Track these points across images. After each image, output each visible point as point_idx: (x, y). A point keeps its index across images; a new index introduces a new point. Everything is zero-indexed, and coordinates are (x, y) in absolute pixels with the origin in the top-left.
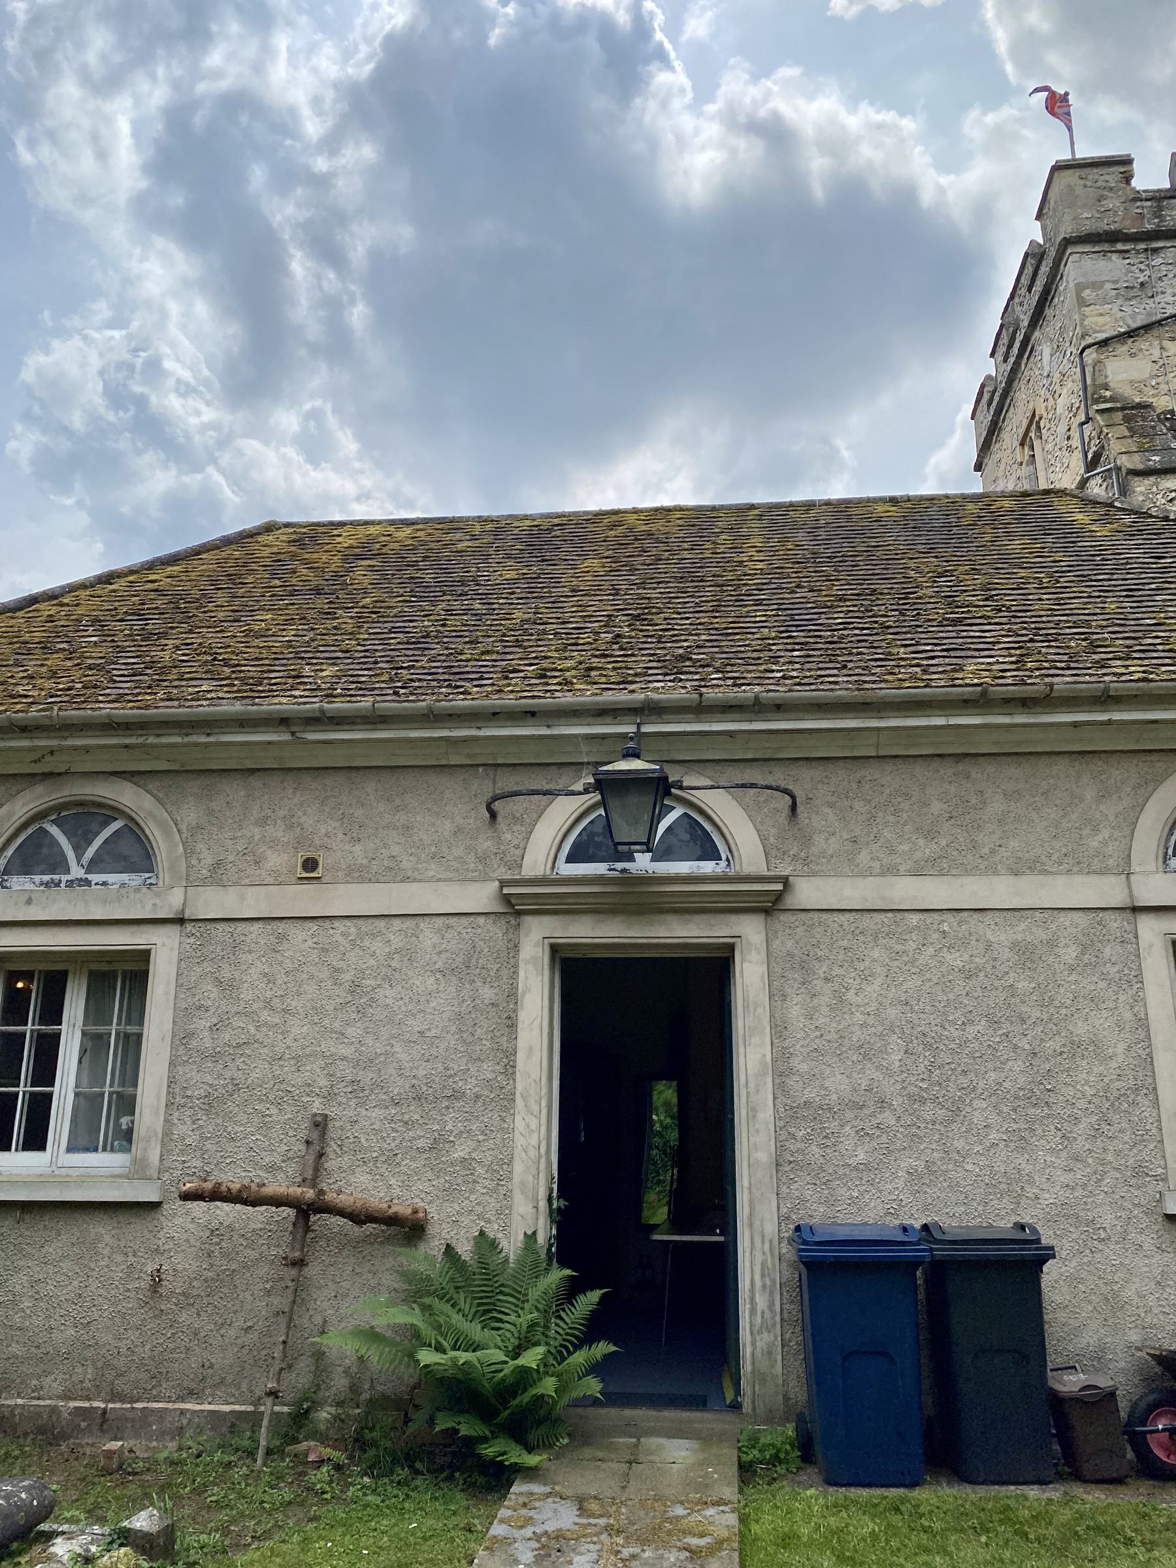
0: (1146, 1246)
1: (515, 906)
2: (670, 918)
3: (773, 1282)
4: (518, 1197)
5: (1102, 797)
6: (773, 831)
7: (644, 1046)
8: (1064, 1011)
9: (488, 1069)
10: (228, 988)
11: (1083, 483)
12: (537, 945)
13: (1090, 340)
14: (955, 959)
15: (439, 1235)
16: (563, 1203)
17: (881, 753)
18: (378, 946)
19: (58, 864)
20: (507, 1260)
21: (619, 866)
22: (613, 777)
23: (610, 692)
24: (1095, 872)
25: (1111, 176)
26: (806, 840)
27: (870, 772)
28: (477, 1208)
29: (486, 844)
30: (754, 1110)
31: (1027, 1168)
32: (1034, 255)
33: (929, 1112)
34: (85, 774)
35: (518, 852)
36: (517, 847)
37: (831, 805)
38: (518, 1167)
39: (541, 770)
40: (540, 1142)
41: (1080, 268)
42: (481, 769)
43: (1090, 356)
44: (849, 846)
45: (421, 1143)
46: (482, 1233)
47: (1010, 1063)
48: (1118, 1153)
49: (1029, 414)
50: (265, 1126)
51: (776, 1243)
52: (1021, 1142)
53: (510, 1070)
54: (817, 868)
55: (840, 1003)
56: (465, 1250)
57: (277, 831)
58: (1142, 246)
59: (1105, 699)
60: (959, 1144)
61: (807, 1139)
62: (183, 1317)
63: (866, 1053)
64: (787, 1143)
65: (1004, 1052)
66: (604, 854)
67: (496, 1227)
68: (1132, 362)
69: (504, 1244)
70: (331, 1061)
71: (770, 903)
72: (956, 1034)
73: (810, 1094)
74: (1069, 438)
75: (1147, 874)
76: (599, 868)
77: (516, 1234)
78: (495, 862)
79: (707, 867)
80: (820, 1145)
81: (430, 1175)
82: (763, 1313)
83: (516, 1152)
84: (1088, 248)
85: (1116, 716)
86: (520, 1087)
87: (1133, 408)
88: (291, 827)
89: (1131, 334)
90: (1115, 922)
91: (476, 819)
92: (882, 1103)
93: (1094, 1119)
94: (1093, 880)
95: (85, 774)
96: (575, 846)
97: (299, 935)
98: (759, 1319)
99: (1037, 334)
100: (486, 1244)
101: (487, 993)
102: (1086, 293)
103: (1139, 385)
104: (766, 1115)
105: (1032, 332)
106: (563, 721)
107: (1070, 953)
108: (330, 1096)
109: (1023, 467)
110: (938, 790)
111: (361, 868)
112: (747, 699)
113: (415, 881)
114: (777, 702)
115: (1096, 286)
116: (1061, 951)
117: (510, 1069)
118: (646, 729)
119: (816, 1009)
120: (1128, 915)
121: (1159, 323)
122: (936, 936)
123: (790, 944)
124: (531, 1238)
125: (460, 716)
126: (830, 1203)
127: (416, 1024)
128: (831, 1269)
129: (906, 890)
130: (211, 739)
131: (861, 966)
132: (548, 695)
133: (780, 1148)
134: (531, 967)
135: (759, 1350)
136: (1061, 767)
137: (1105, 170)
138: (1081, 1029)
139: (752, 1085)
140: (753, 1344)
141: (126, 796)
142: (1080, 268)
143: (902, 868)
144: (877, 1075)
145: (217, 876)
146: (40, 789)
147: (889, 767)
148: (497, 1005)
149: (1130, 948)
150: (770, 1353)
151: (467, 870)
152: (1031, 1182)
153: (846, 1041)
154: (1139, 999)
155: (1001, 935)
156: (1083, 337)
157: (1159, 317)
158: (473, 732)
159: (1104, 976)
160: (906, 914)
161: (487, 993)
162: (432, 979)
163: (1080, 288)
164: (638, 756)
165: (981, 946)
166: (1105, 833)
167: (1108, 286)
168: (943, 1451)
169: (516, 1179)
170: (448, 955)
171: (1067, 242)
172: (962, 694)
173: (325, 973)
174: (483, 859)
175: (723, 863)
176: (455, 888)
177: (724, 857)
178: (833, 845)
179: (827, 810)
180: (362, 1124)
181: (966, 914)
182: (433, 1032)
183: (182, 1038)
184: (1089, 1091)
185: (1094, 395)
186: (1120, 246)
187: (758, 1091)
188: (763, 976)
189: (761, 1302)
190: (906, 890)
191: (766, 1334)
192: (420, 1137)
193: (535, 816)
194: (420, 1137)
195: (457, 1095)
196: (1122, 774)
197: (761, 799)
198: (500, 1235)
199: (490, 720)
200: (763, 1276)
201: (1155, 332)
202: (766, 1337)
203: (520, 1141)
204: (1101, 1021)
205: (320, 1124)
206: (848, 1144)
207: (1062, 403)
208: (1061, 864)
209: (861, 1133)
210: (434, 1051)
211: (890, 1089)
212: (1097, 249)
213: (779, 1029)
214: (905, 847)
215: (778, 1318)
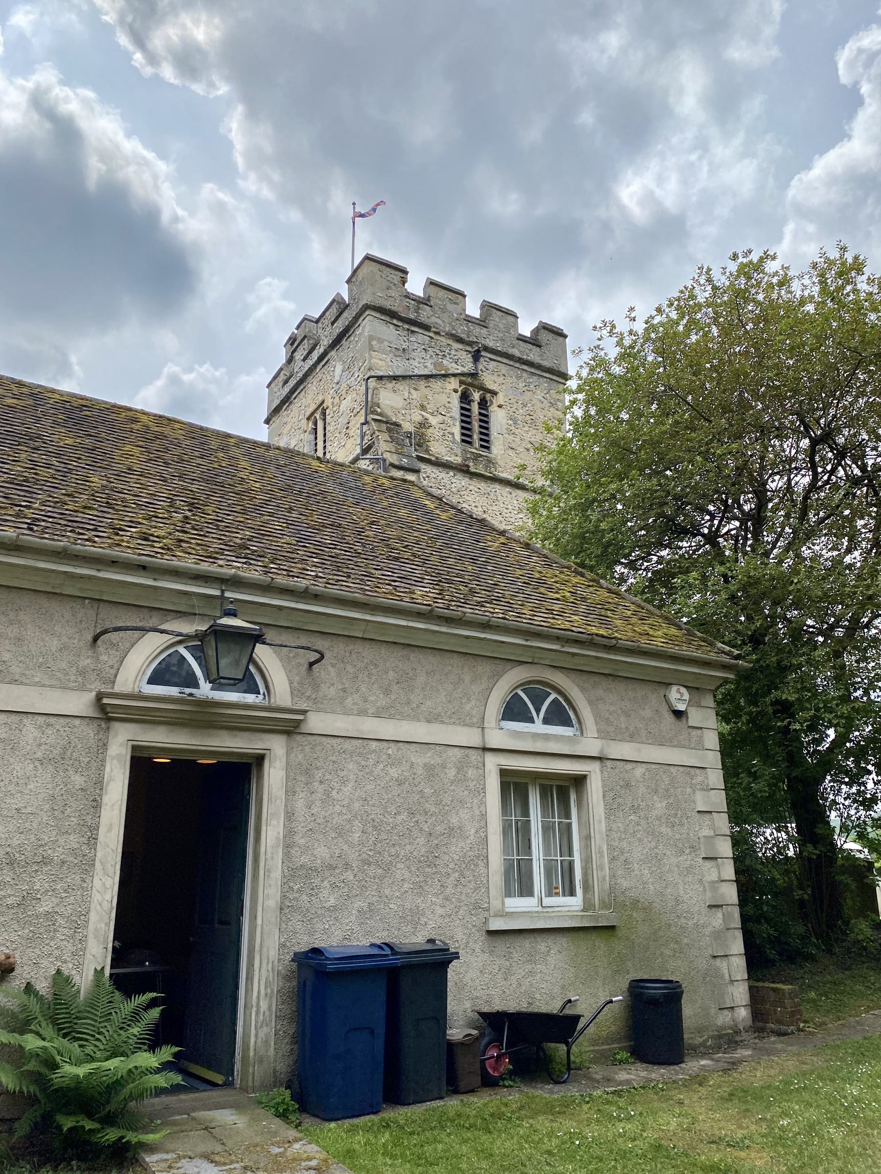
0: (477, 950)
1: (106, 712)
2: (224, 733)
3: (272, 990)
5: (473, 682)
6: (297, 678)
8: (447, 808)
9: (73, 840)
11: (356, 460)
12: (121, 745)
13: (373, 374)
14: (394, 772)
16: (117, 944)
17: (366, 636)
20: (79, 992)
21: (188, 690)
22: (227, 629)
23: (206, 564)
24: (466, 725)
25: (396, 277)
26: (316, 687)
27: (358, 647)
28: (56, 951)
29: (86, 662)
30: (269, 871)
32: (338, 303)
33: (372, 871)
35: (113, 671)
36: (112, 667)
37: (333, 666)
38: (93, 917)
39: (151, 610)
40: (112, 897)
41: (370, 325)
42: (87, 601)
43: (372, 383)
44: (341, 694)
45: (10, 901)
46: (59, 972)
47: (418, 840)
48: (467, 895)
49: (318, 403)
51: (276, 963)
52: (419, 888)
53: (93, 841)
54: (321, 706)
56: (43, 986)
58: (406, 326)
59: (486, 626)
60: (387, 892)
63: (341, 832)
64: (287, 894)
65: (415, 833)
66: (176, 680)
67: (71, 966)
68: (393, 395)
69: (76, 979)
71: (290, 728)
72: (391, 820)
73: (304, 859)
74: (347, 428)
75: (492, 729)
76: (173, 691)
77: (88, 970)
78: (93, 677)
79: (250, 698)
80: (300, 894)
81: (16, 927)
82: (264, 1013)
83: (92, 907)
84: (378, 315)
86: (99, 854)
87: (391, 424)
89: (395, 378)
90: (474, 756)
91: (80, 640)
92: (347, 866)
93: (457, 875)
96: (155, 672)
98: (261, 1017)
99: (333, 353)
100: (60, 980)
101: (78, 780)
102: (374, 343)
103: (397, 411)
104: (277, 874)
105: (330, 351)
106: (167, 577)
107: (452, 773)
109: (306, 434)
110: (392, 662)
112: (300, 587)
113: (22, 683)
114: (318, 593)
115: (381, 341)
116: (447, 771)
117: (92, 840)
119: (313, 802)
120: (480, 752)
121: (410, 377)
122: (384, 757)
123: (300, 756)
124: (99, 973)
125: (84, 557)
126: (311, 934)
128: (317, 977)
129: (372, 727)
131: (342, 774)
132: (159, 555)
133: (284, 897)
134: (115, 762)
135: (259, 1040)
136: (456, 660)
137: (393, 272)
139: (269, 854)
140: (256, 1036)
142: (370, 325)
143: (370, 711)
144: (345, 847)
147: (367, 645)
148: (86, 790)
149: (481, 772)
150: (266, 1041)
151: (69, 680)
152: (423, 915)
153: (329, 824)
154: (483, 803)
155: (420, 759)
156: (369, 369)
157: (411, 373)
158: (93, 573)
160: (370, 742)
161: (78, 780)
162: (31, 766)
163: (371, 338)
164: (235, 615)
165: (408, 766)
166: (473, 702)
167: (386, 343)
168: (395, 1088)
169: (91, 926)
170: (47, 747)
171: (367, 307)
172: (419, 609)
174: (82, 673)
175: (261, 697)
176: (57, 694)
177: (262, 692)
178: (332, 692)
179: (331, 669)
181: (401, 744)
182: (29, 810)
185: (370, 407)
186: (395, 321)
187: (272, 858)
188: (282, 778)
189: (264, 1005)
190: (372, 727)
191: (265, 1028)
192: (10, 896)
193: (128, 645)
194: (10, 896)
195: (45, 861)
196: (485, 668)
197: (291, 655)
198: (74, 972)
199: (110, 566)
200: (266, 988)
201: (407, 381)
202: (265, 1029)
203: (96, 897)
206: (325, 893)
207: (346, 405)
208: (450, 718)
209: (334, 886)
210: (27, 825)
211: (353, 856)
212: (383, 318)
213: (290, 816)
214: (372, 698)
215: (274, 1016)
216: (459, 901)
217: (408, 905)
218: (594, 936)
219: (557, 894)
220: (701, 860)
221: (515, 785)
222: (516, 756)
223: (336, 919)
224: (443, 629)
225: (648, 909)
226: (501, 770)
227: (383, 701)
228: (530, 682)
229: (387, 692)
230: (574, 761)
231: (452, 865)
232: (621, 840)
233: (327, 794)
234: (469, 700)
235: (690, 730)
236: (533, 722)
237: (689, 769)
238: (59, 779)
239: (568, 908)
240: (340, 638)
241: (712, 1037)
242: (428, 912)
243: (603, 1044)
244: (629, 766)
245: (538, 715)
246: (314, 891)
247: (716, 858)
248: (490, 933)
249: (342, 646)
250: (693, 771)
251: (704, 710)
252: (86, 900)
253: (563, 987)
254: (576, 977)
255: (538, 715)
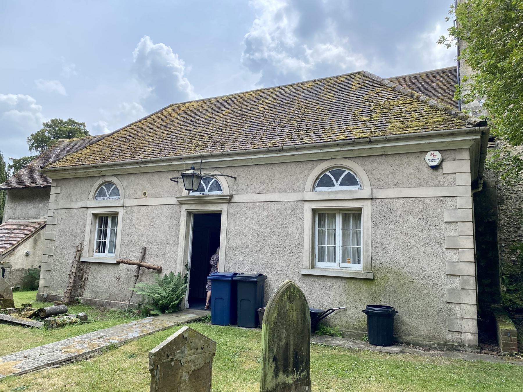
2: (210, 205)
4: (178, 265)
7: (206, 232)
9: (174, 238)
10: (131, 220)
14: (265, 213)
15: (164, 272)
18: (156, 212)
19: (105, 195)
21: (202, 193)
29: (176, 189)
31: (274, 262)
33: (256, 249)
34: (108, 176)
38: (178, 259)
44: (246, 187)
45: (162, 253)
50: (136, 249)
52: (274, 256)
55: (241, 224)
57: (139, 187)
61: (232, 254)
62: (123, 286)
63: (245, 235)
70: (147, 236)
71: (229, 200)
73: (233, 244)
79: (219, 193)
85: (300, 153)
88: (142, 186)
94: (296, 194)
95: (108, 176)
97: (143, 209)
107: (289, 212)
108: (147, 243)
110: (265, 172)
111: (153, 195)
118: (203, 161)
126: (235, 268)
127: (162, 228)
130: (322, 151)
138: (289, 230)
141: (114, 180)
145: (129, 197)
146: (101, 179)
147: (256, 167)
154: (303, 223)
155: (275, 207)
159: (296, 217)
161: (175, 222)
166: (301, 182)
169: (178, 261)
173: (147, 217)
178: (243, 186)
180: (152, 249)
183: (123, 231)
184: (290, 245)
195: (168, 243)
203: (179, 253)
204: (294, 228)
205: (145, 249)
209: (242, 253)
211: (249, 243)
216: (290, 261)
217: (269, 261)
218: (360, 282)
219: (349, 262)
220: (444, 250)
221: (321, 216)
222: (322, 202)
223: (243, 264)
224: (279, 155)
225: (398, 274)
226: (313, 209)
227: (262, 187)
228: (333, 167)
229: (263, 184)
230: (354, 201)
231: (287, 248)
232: (382, 238)
233: (241, 222)
234: (299, 181)
235: (445, 175)
236: (333, 185)
237: (441, 198)
238: (171, 222)
239: (356, 269)
240: (304, 163)
241: (437, 344)
242: (277, 265)
243: (361, 330)
244: (393, 200)
245: (337, 182)
246: (236, 255)
247: (458, 249)
248: (303, 275)
249: (246, 169)
250: (444, 199)
251: (457, 161)
252: (177, 254)
253: (340, 302)
254: (347, 299)
255: (337, 182)
